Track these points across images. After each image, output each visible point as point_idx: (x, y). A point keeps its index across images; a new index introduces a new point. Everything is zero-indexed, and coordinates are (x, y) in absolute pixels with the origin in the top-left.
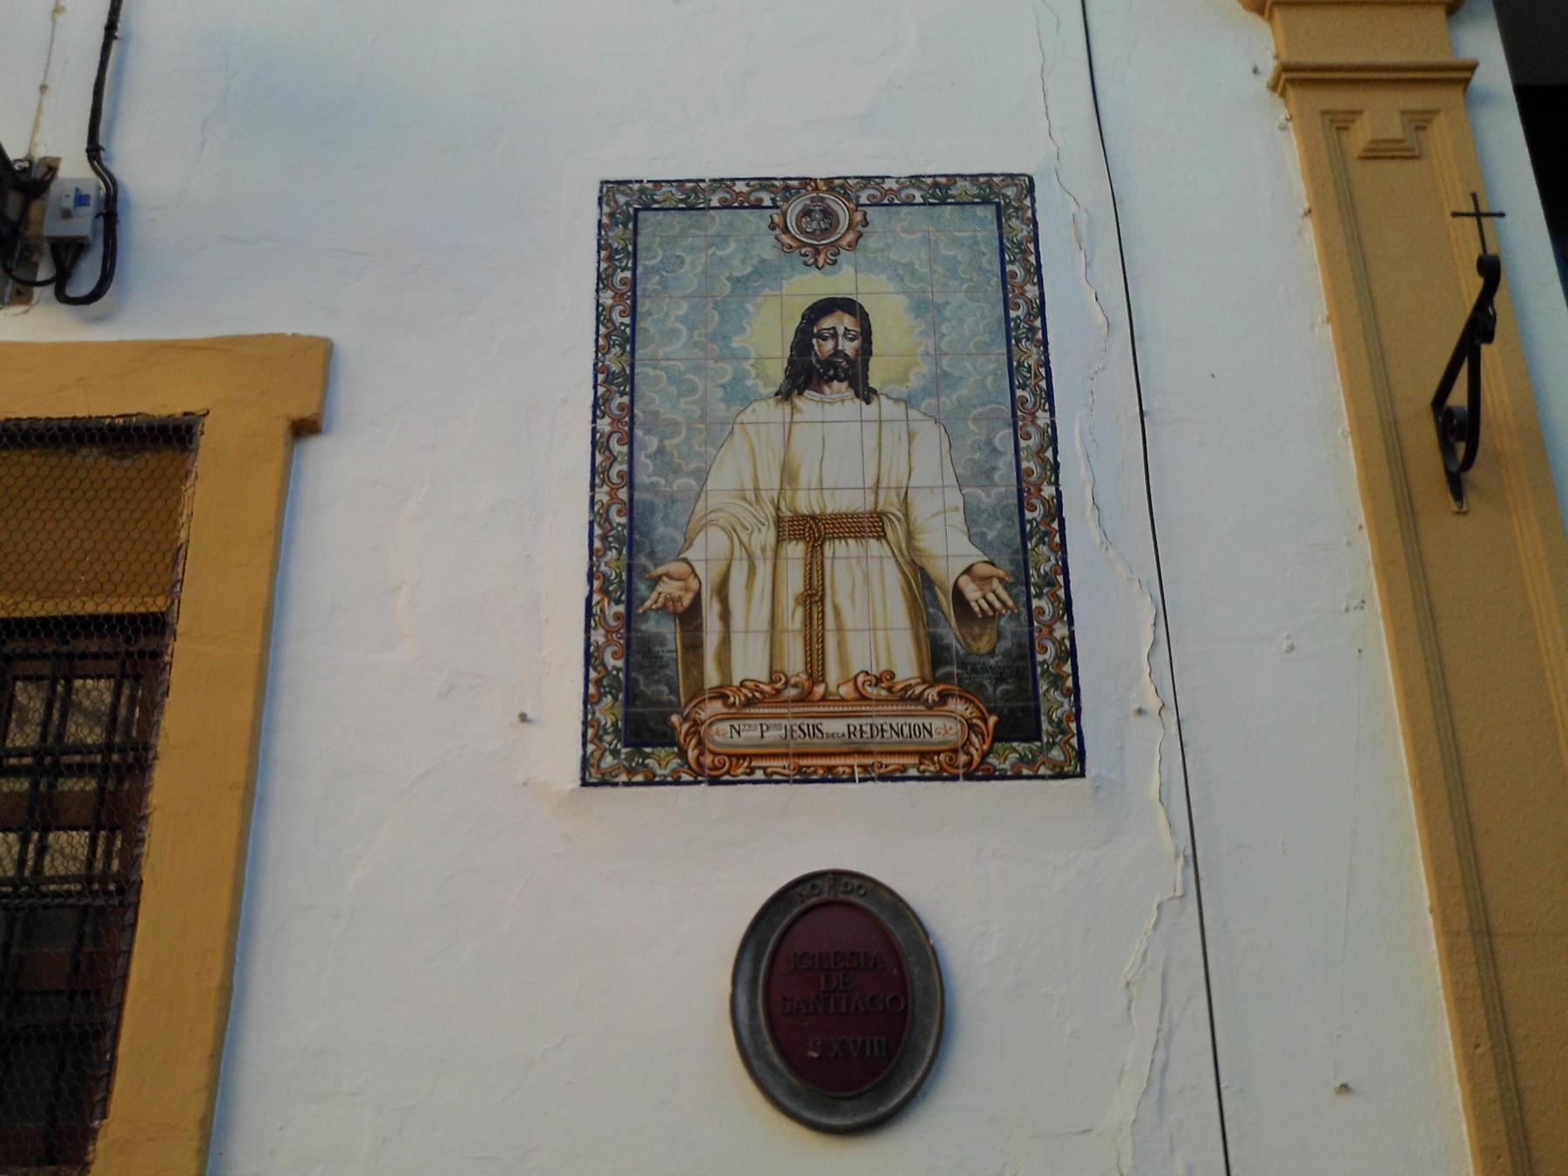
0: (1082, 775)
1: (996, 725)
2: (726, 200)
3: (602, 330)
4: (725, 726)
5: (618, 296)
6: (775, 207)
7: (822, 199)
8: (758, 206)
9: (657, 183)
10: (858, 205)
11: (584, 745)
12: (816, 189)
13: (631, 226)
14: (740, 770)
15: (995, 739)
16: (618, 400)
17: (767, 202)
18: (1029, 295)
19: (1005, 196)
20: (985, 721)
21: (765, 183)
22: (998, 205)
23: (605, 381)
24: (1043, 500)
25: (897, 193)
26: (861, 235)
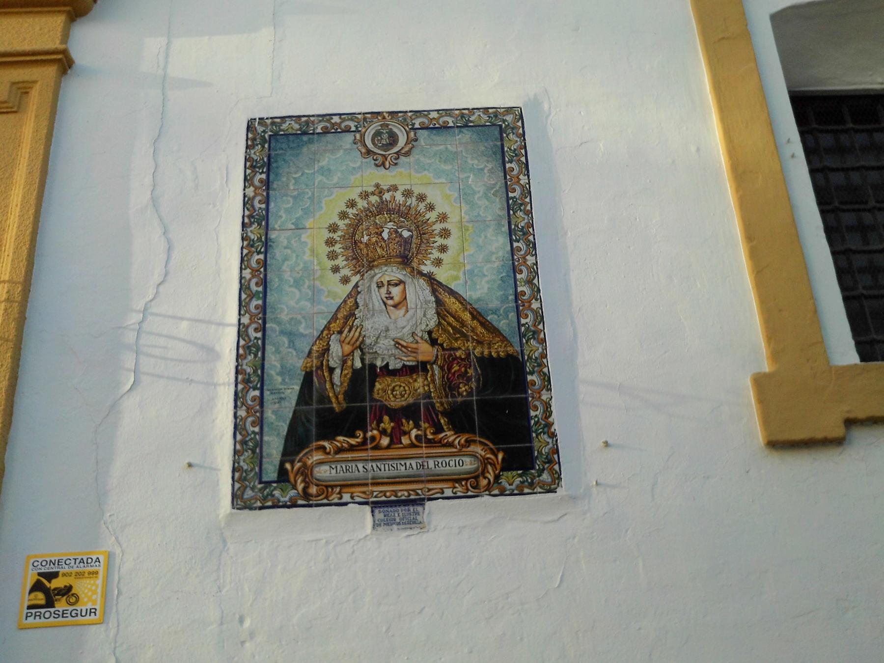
0: (500, 135)
1: (503, 459)
2: (326, 128)
3: (242, 343)
4: (325, 468)
5: (255, 272)
6: (357, 131)
7: (387, 125)
8: (348, 130)
9: (283, 118)
10: (413, 129)
11: (236, 386)
12: (384, 118)
13: (260, 354)
14: (334, 496)
15: (502, 470)
16: (259, 177)
17: (353, 129)
18: (522, 182)
19: (504, 121)
20: (496, 457)
21: (352, 116)
22: (501, 126)
23: (248, 245)
24: (532, 310)
25: (437, 119)
26: (413, 147)
